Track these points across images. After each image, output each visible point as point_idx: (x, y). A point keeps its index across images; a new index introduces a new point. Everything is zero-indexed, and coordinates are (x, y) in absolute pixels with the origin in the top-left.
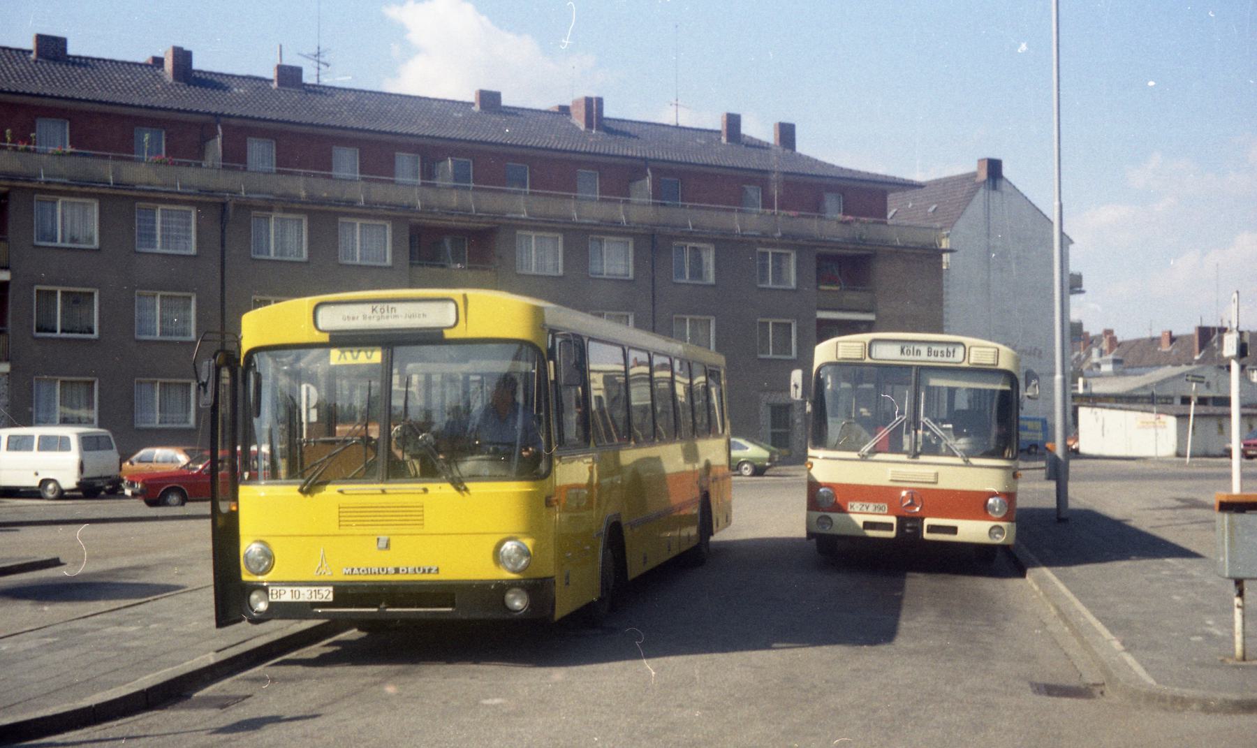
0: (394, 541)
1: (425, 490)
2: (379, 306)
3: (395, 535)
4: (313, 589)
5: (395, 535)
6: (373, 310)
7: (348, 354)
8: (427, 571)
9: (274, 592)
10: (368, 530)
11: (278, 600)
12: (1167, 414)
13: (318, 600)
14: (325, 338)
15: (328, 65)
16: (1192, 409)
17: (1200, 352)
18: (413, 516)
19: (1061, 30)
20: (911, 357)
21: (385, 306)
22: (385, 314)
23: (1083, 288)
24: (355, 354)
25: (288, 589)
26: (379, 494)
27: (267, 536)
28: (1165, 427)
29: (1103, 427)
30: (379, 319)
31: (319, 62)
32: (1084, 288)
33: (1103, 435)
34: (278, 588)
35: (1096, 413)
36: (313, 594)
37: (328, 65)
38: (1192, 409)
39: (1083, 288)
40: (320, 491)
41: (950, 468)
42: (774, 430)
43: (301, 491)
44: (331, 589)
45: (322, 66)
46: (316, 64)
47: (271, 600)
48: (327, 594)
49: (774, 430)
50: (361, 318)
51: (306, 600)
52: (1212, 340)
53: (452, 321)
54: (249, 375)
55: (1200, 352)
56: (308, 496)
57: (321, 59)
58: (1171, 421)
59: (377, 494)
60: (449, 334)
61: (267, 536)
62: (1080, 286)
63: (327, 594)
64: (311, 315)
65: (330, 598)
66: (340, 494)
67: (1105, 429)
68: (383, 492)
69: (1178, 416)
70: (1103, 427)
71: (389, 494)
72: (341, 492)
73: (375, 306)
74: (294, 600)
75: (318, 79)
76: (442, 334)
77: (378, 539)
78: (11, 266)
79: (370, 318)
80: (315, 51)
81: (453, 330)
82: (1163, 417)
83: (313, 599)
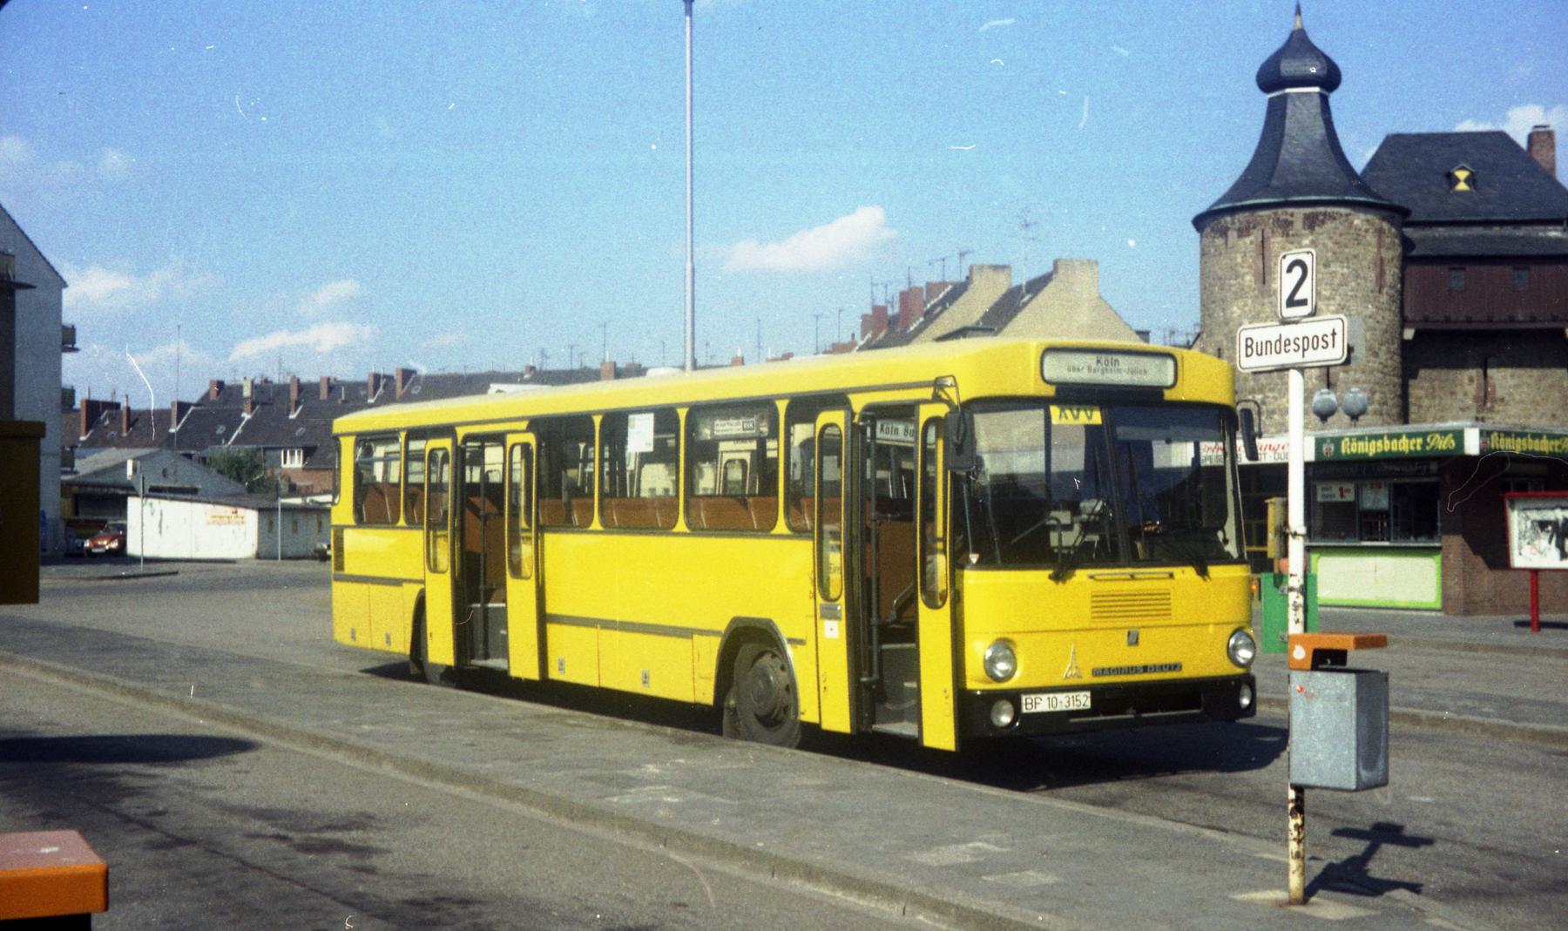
0: (1143, 635)
1: (1171, 576)
2: (1103, 357)
3: (1144, 627)
4: (1071, 695)
5: (1144, 627)
6: (1098, 361)
7: (1082, 413)
9: (1029, 701)
10: (1120, 623)
11: (1033, 710)
12: (246, 507)
13: (1075, 708)
14: (1050, 391)
17: (87, 430)
18: (1160, 604)
20: (889, 436)
21: (1109, 357)
22: (1110, 367)
23: (77, 346)
24: (1089, 413)
25: (1045, 697)
26: (1128, 580)
27: (1014, 633)
28: (243, 522)
29: (161, 522)
30: (1103, 373)
32: (77, 345)
33: (160, 532)
34: (1033, 697)
35: (151, 504)
39: (77, 346)
40: (1070, 577)
43: (1050, 577)
44: (1088, 694)
48: (1084, 700)
50: (1086, 370)
51: (1064, 708)
52: (102, 418)
53: (1170, 381)
55: (87, 430)
56: (1061, 584)
58: (251, 517)
59: (1163, 578)
60: (1169, 395)
61: (1014, 633)
62: (73, 342)
63: (1084, 700)
64: (1039, 359)
65: (1088, 704)
66: (1092, 580)
67: (164, 525)
68: (1132, 577)
69: (260, 510)
70: (161, 522)
71: (1140, 579)
72: (1092, 577)
73: (1099, 356)
74: (1052, 709)
79: (1095, 371)
81: (1173, 391)
82: (241, 511)
83: (1071, 708)
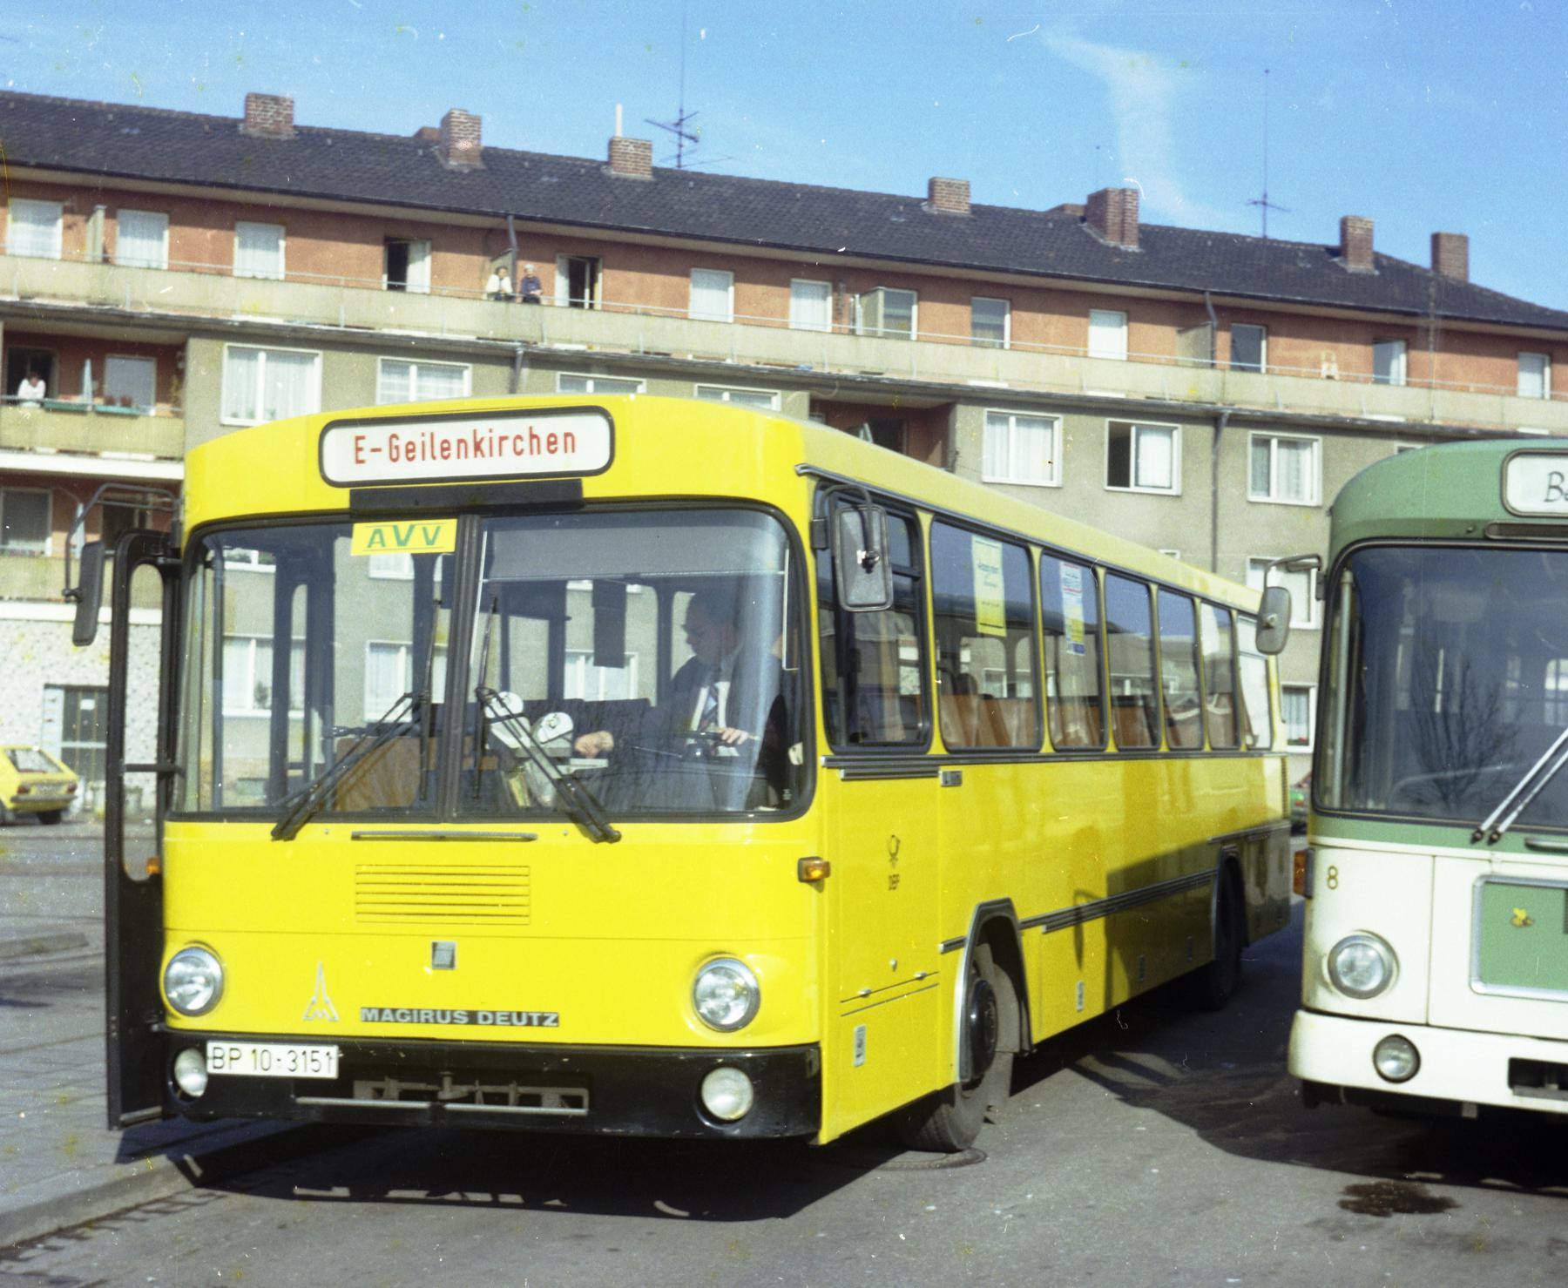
8: (535, 1022)
15: (693, 138)
16: (664, 753)
19: (1531, 891)
31: (680, 134)
36: (301, 1059)
37: (693, 138)
38: (664, 753)
41: (1411, 550)
42: (70, 744)
45: (686, 142)
46: (675, 137)
47: (211, 1070)
49: (70, 744)
54: (1396, 650)
57: (686, 130)
60: (592, 489)
63: (324, 1063)
75: (679, 162)
76: (577, 487)
77: (435, 946)
78: (187, 459)
80: (675, 117)
83: (300, 1073)
